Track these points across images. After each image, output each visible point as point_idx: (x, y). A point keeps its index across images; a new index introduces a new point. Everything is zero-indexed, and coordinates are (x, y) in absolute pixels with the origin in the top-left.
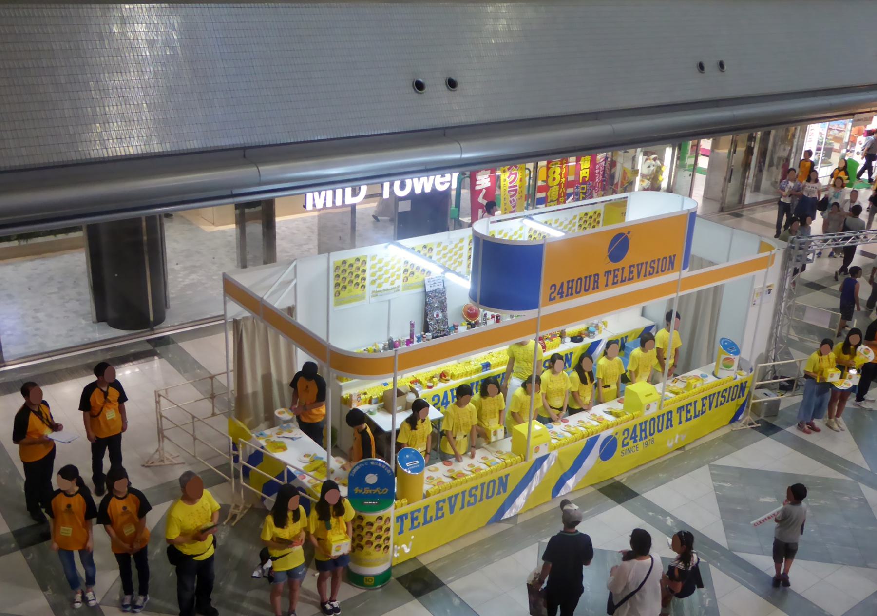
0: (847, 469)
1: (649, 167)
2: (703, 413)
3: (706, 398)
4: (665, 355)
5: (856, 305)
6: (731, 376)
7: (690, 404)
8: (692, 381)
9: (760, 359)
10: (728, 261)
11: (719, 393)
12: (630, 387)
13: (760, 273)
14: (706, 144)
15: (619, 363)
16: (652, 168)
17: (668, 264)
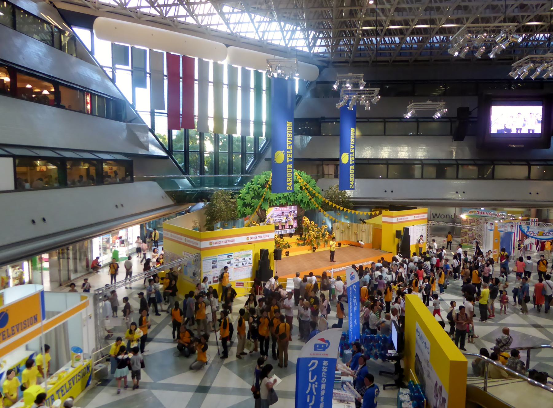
0: (455, 333)
1: (16, 273)
2: (70, 388)
3: (70, 380)
4: (43, 367)
5: (488, 311)
6: (81, 365)
7: (63, 387)
8: (62, 375)
9: (93, 351)
10: (67, 308)
11: (76, 375)
12: (26, 391)
13: (83, 311)
14: (45, 256)
15: (16, 380)
16: (18, 273)
17: (35, 320)
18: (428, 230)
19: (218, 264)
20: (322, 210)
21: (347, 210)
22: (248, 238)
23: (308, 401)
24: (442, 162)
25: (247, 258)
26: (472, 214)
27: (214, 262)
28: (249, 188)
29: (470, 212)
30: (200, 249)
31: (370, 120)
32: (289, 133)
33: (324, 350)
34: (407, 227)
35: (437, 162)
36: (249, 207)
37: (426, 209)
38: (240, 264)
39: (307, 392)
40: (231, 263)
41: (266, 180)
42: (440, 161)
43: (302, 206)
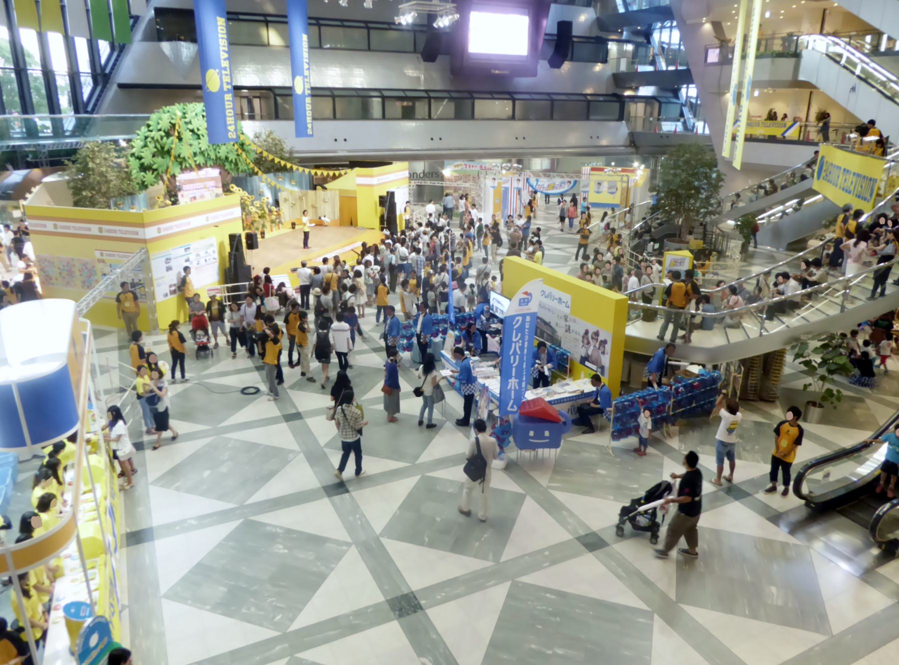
18: (410, 194)
19: (173, 264)
20: (260, 173)
21: (304, 171)
22: (207, 219)
23: (512, 362)
25: (210, 251)
26: (457, 169)
27: (168, 260)
28: (146, 138)
29: (455, 166)
30: (144, 241)
31: (346, 24)
32: (223, 38)
33: (527, 305)
34: (391, 190)
36: (151, 172)
37: (405, 164)
38: (202, 261)
39: (511, 353)
40: (191, 260)
41: (170, 123)
42: (406, 92)
43: (227, 166)
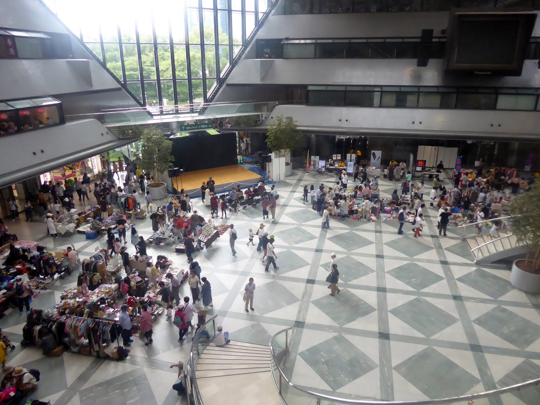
24: (403, 89)
35: (397, 89)
